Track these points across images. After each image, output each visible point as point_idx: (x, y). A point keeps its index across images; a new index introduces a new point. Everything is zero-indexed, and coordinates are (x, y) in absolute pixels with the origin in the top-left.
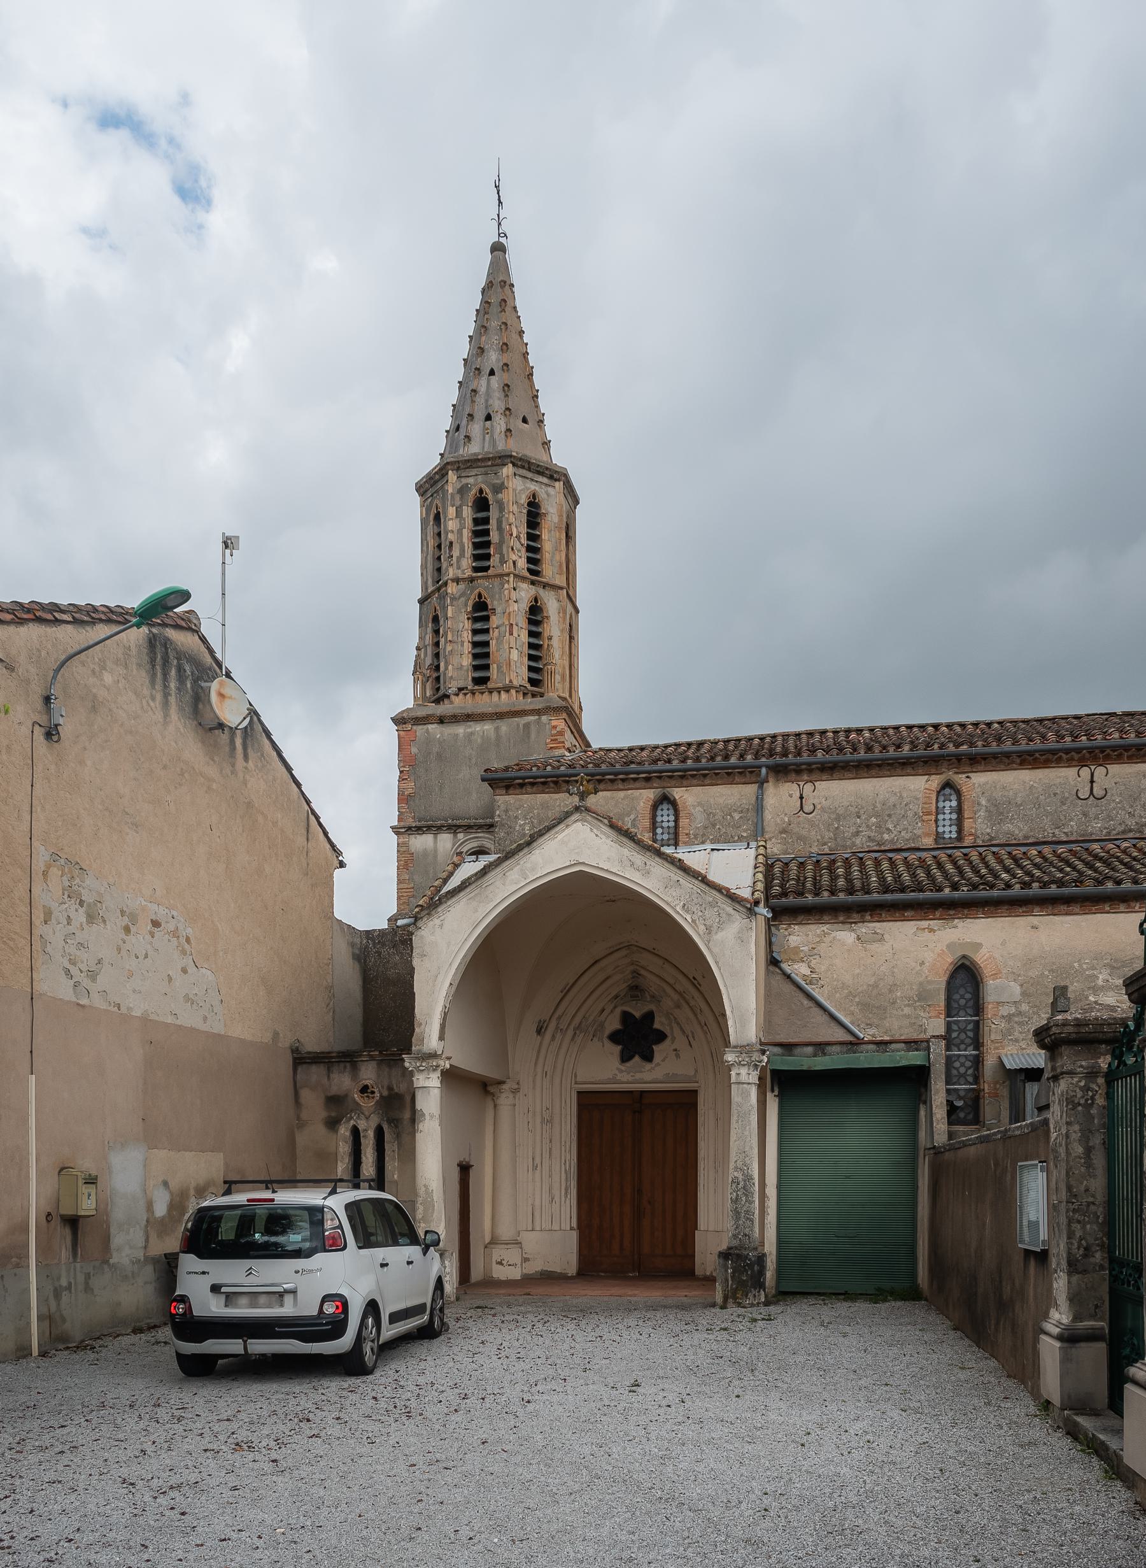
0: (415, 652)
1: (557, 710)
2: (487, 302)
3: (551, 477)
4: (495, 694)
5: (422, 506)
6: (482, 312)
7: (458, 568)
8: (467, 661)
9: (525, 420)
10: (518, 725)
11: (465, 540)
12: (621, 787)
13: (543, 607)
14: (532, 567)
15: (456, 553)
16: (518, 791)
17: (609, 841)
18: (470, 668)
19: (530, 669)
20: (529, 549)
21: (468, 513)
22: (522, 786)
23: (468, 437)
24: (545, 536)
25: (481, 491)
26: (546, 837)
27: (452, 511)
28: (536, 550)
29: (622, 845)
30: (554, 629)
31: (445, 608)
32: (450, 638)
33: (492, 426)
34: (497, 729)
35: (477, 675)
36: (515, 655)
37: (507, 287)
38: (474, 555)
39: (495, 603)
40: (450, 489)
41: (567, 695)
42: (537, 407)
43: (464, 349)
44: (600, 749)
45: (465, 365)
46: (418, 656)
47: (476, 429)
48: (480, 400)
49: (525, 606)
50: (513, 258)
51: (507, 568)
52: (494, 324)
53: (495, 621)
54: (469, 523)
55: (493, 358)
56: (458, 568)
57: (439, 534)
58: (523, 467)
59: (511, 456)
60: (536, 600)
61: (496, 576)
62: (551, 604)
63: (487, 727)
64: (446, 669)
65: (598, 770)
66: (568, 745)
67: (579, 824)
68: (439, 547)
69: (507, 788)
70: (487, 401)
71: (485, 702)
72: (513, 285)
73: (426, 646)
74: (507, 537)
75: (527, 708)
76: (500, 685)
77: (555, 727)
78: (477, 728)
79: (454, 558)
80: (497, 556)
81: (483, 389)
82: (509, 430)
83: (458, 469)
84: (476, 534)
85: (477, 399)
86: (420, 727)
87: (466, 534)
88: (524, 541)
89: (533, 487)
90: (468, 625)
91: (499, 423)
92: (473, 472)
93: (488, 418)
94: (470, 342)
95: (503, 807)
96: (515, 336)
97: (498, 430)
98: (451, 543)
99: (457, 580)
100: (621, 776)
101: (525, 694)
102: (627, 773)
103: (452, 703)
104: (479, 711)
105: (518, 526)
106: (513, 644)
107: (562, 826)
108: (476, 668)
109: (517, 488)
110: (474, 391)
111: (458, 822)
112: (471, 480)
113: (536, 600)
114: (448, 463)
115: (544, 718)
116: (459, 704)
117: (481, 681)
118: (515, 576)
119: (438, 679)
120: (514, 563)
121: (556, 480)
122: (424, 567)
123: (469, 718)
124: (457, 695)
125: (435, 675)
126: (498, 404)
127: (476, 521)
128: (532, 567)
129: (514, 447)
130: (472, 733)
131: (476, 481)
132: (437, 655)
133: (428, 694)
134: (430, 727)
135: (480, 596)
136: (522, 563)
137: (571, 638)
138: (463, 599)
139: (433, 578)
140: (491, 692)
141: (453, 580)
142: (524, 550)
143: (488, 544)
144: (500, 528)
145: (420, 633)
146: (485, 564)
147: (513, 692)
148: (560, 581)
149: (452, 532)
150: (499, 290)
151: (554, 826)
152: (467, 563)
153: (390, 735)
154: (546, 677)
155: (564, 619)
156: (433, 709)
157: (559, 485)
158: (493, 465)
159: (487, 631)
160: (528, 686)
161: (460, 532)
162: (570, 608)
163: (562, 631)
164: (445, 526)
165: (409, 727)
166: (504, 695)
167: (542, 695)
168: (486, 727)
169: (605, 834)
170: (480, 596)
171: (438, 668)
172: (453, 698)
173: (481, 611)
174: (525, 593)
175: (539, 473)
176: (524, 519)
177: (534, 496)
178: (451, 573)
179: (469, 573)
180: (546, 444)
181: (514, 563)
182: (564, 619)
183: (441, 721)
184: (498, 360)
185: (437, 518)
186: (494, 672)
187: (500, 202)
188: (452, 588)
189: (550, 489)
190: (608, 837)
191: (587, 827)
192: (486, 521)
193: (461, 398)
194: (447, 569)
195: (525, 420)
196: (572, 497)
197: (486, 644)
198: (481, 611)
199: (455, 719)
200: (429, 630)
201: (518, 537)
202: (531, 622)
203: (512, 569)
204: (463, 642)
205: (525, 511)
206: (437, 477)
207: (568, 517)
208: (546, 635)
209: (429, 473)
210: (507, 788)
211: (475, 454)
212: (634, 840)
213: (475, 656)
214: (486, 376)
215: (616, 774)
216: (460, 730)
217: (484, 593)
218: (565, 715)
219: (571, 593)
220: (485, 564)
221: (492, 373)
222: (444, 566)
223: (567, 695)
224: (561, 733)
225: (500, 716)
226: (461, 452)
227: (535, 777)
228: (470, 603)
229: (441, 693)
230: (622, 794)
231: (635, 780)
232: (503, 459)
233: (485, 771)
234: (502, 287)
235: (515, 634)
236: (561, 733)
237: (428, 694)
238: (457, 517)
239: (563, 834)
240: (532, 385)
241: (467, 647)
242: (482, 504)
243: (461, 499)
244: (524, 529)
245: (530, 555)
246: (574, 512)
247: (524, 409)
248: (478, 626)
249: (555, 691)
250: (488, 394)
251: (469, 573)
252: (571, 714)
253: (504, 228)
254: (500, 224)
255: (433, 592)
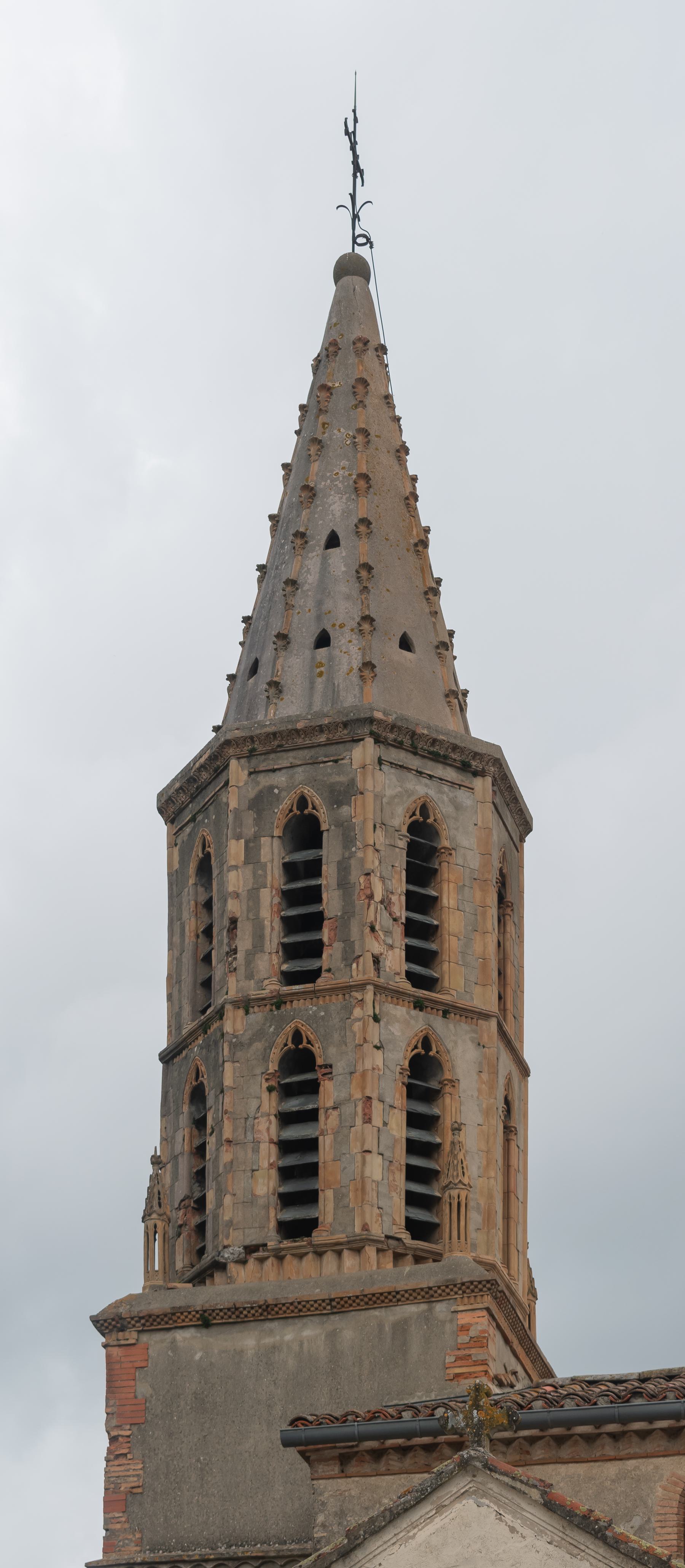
0: (149, 1170)
1: (469, 1288)
2: (324, 388)
3: (464, 767)
4: (329, 1259)
5: (171, 845)
6: (313, 411)
7: (250, 976)
8: (266, 1185)
9: (405, 644)
10: (381, 1326)
11: (265, 913)
12: (609, 1451)
13: (443, 1058)
14: (417, 969)
15: (244, 943)
16: (367, 1468)
17: (541, 1544)
18: (274, 1199)
19: (412, 1199)
20: (411, 929)
21: (273, 853)
22: (377, 1455)
23: (275, 685)
24: (449, 897)
25: (303, 802)
26: (388, 1535)
27: (235, 850)
28: (429, 932)
29: (574, 1550)
30: (467, 1107)
31: (217, 1068)
32: (227, 1134)
33: (331, 658)
34: (332, 1336)
35: (290, 1215)
36: (375, 1168)
37: (371, 353)
38: (285, 946)
39: (332, 1051)
40: (232, 800)
41: (496, 1258)
42: (436, 613)
43: (271, 494)
44: (574, 1380)
45: (274, 529)
46: (155, 1179)
47: (295, 666)
48: (305, 601)
49: (399, 1057)
50: (385, 290)
51: (362, 971)
52: (339, 435)
53: (330, 1092)
54: (275, 876)
55: (335, 509)
56: (250, 976)
57: (208, 905)
58: (399, 745)
59: (371, 720)
60: (426, 1043)
61: (334, 990)
62: (463, 1053)
63: (309, 1333)
64: (219, 1204)
65: (555, 1413)
66: (495, 1369)
67: (469, 1503)
68: (208, 932)
69: (344, 1460)
70: (320, 603)
71: (306, 1276)
72: (383, 349)
73: (176, 1158)
74: (360, 902)
75: (401, 1286)
76: (341, 1237)
77: (464, 1328)
78: (288, 1334)
79: (240, 955)
80: (338, 945)
81: (310, 579)
82: (368, 665)
83: (251, 754)
84: (290, 898)
85: (298, 600)
86: (158, 1336)
87: (269, 899)
88: (402, 913)
89: (421, 789)
90: (270, 1104)
91: (348, 651)
92: (285, 760)
93: (323, 640)
94: (286, 478)
95: (333, 1506)
96: (388, 459)
97: (345, 668)
98: (234, 921)
99: (246, 1004)
100: (612, 1428)
101: (398, 1257)
102: (624, 1420)
103: (231, 1280)
104: (292, 1297)
105: (385, 878)
106: (371, 1143)
107: (426, 1508)
108: (287, 1200)
109: (384, 793)
110: (292, 583)
111: (239, 1551)
112: (280, 779)
113: (426, 1043)
114: (227, 743)
115: (441, 1309)
116: (245, 1282)
117: (297, 1229)
118: (379, 989)
119: (201, 1229)
120: (376, 960)
121: (475, 774)
122: (173, 980)
123: (268, 1312)
124: (243, 1262)
125: (195, 1220)
126: (344, 610)
127: (291, 870)
128: (417, 969)
129: (379, 700)
130: (275, 1348)
131: (290, 780)
132: (200, 1176)
133: (179, 1265)
134: (180, 1336)
135: (297, 1036)
136: (395, 961)
137: (509, 1130)
138: (258, 1046)
139: (193, 1004)
140: (320, 1254)
141: (236, 1004)
142: (398, 930)
143: (316, 921)
144: (344, 884)
145: (164, 1129)
146: (311, 964)
147: (370, 1251)
148: (485, 999)
149: (237, 895)
150: (352, 359)
151: (407, 1509)
152: (269, 964)
153: (86, 1364)
154: (445, 1217)
155: (492, 1087)
156: (187, 1295)
157: (483, 786)
158: (329, 743)
159: (311, 1116)
160: (406, 1236)
161: (253, 895)
162: (506, 1063)
163: (487, 1113)
164: (222, 884)
165: (131, 1336)
166: (349, 1260)
167: (437, 1257)
168: (307, 1333)
169: (532, 1525)
170: (297, 1036)
171: (201, 1204)
172: (232, 1268)
173: (299, 1073)
174: (402, 1027)
175: (436, 758)
176: (401, 860)
177: (424, 809)
178: (233, 987)
179: (273, 986)
180: (457, 698)
181: (376, 960)
182: (492, 1087)
183: (206, 1320)
184: (346, 513)
185: (205, 868)
186: (326, 1208)
187: (357, 169)
188: (234, 1023)
189: (462, 796)
190: (540, 1533)
191: (488, 1511)
192: (314, 868)
193: (264, 602)
194: (224, 982)
195: (405, 644)
196: (516, 818)
197: (311, 1145)
198: (299, 1073)
199: (237, 1316)
200: (184, 1120)
201: (386, 903)
202: (412, 1093)
203: (371, 974)
204: (257, 1143)
205: (403, 844)
206: (205, 776)
207: (504, 858)
208: (447, 1122)
209: (188, 768)
210: (344, 1460)
211: (290, 720)
212: (604, 1540)
213: (286, 1174)
214: (319, 550)
215: (598, 1422)
216: (248, 1340)
217: (307, 1031)
218: (487, 1300)
219: (509, 1029)
220: (311, 964)
221: (333, 541)
222: (218, 970)
223: (496, 1258)
224: (480, 1342)
225: (337, 1306)
226: (260, 717)
227: (409, 1435)
228: (276, 1055)
229: (207, 1258)
230: (611, 1469)
231: (643, 1435)
232: (353, 727)
233: (293, 1422)
234: (359, 353)
235: (377, 1121)
236: (480, 1342)
237: (179, 1265)
238: (247, 862)
239: (431, 1528)
240: (425, 567)
241: (268, 1155)
242: (305, 831)
243: (258, 821)
244: (399, 885)
245: (415, 942)
246: (519, 849)
247: (406, 618)
248: (294, 1105)
249: (468, 1248)
250: (323, 587)
251: (273, 986)
252: (511, 1310)
253: (365, 224)
254: (355, 217)
255: (193, 1034)
